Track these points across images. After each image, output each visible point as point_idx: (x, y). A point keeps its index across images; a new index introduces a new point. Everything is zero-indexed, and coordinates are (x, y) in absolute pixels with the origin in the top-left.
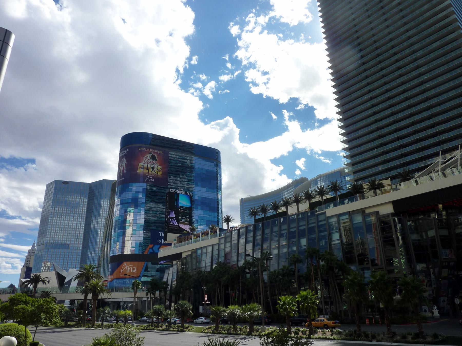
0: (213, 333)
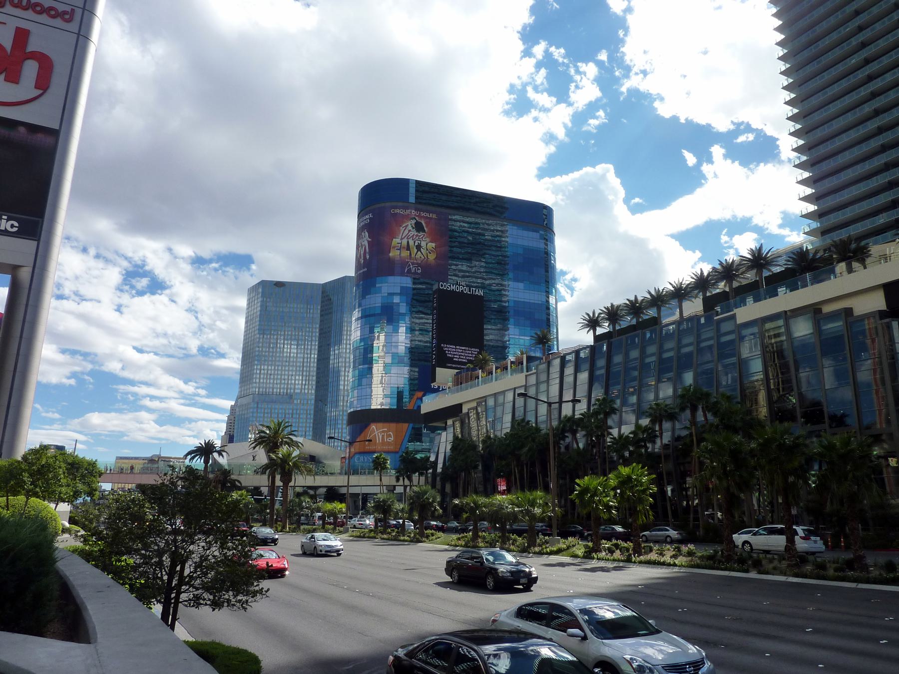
0: (629, 560)
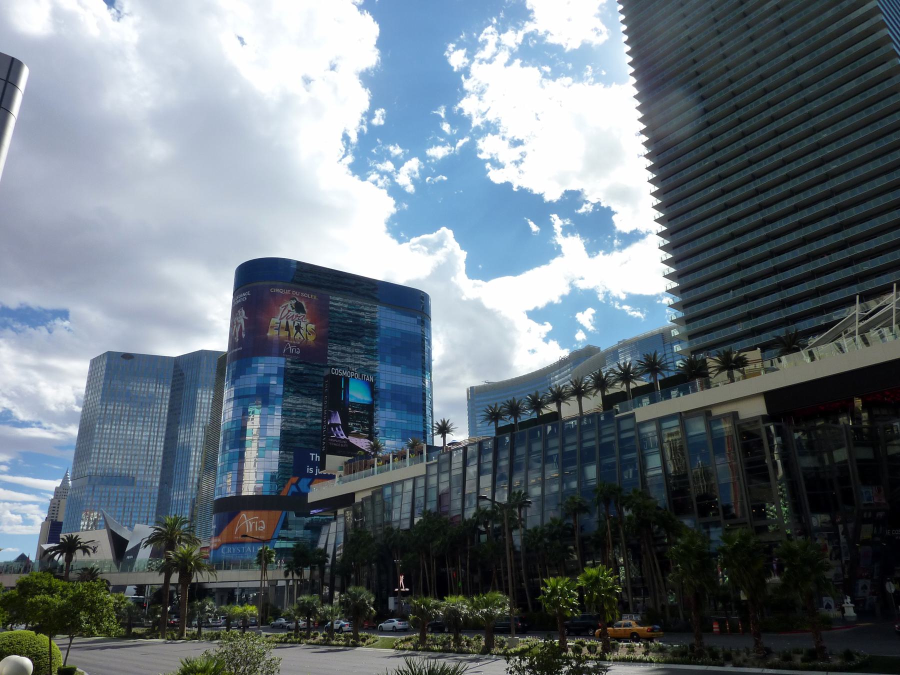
0: (416, 649)
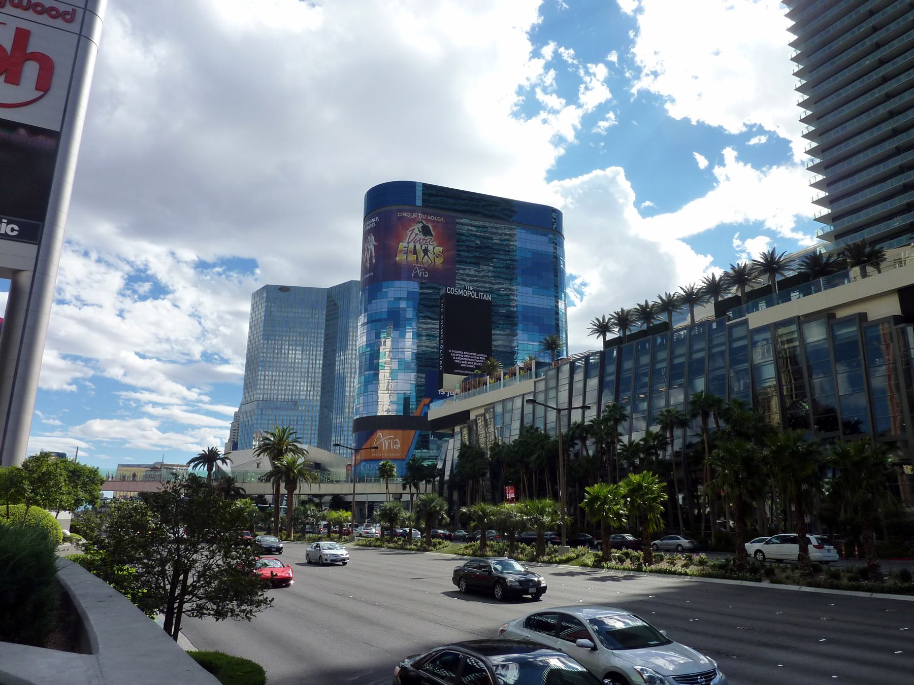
0: (639, 569)
